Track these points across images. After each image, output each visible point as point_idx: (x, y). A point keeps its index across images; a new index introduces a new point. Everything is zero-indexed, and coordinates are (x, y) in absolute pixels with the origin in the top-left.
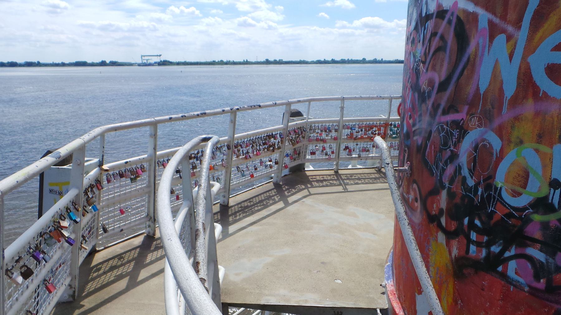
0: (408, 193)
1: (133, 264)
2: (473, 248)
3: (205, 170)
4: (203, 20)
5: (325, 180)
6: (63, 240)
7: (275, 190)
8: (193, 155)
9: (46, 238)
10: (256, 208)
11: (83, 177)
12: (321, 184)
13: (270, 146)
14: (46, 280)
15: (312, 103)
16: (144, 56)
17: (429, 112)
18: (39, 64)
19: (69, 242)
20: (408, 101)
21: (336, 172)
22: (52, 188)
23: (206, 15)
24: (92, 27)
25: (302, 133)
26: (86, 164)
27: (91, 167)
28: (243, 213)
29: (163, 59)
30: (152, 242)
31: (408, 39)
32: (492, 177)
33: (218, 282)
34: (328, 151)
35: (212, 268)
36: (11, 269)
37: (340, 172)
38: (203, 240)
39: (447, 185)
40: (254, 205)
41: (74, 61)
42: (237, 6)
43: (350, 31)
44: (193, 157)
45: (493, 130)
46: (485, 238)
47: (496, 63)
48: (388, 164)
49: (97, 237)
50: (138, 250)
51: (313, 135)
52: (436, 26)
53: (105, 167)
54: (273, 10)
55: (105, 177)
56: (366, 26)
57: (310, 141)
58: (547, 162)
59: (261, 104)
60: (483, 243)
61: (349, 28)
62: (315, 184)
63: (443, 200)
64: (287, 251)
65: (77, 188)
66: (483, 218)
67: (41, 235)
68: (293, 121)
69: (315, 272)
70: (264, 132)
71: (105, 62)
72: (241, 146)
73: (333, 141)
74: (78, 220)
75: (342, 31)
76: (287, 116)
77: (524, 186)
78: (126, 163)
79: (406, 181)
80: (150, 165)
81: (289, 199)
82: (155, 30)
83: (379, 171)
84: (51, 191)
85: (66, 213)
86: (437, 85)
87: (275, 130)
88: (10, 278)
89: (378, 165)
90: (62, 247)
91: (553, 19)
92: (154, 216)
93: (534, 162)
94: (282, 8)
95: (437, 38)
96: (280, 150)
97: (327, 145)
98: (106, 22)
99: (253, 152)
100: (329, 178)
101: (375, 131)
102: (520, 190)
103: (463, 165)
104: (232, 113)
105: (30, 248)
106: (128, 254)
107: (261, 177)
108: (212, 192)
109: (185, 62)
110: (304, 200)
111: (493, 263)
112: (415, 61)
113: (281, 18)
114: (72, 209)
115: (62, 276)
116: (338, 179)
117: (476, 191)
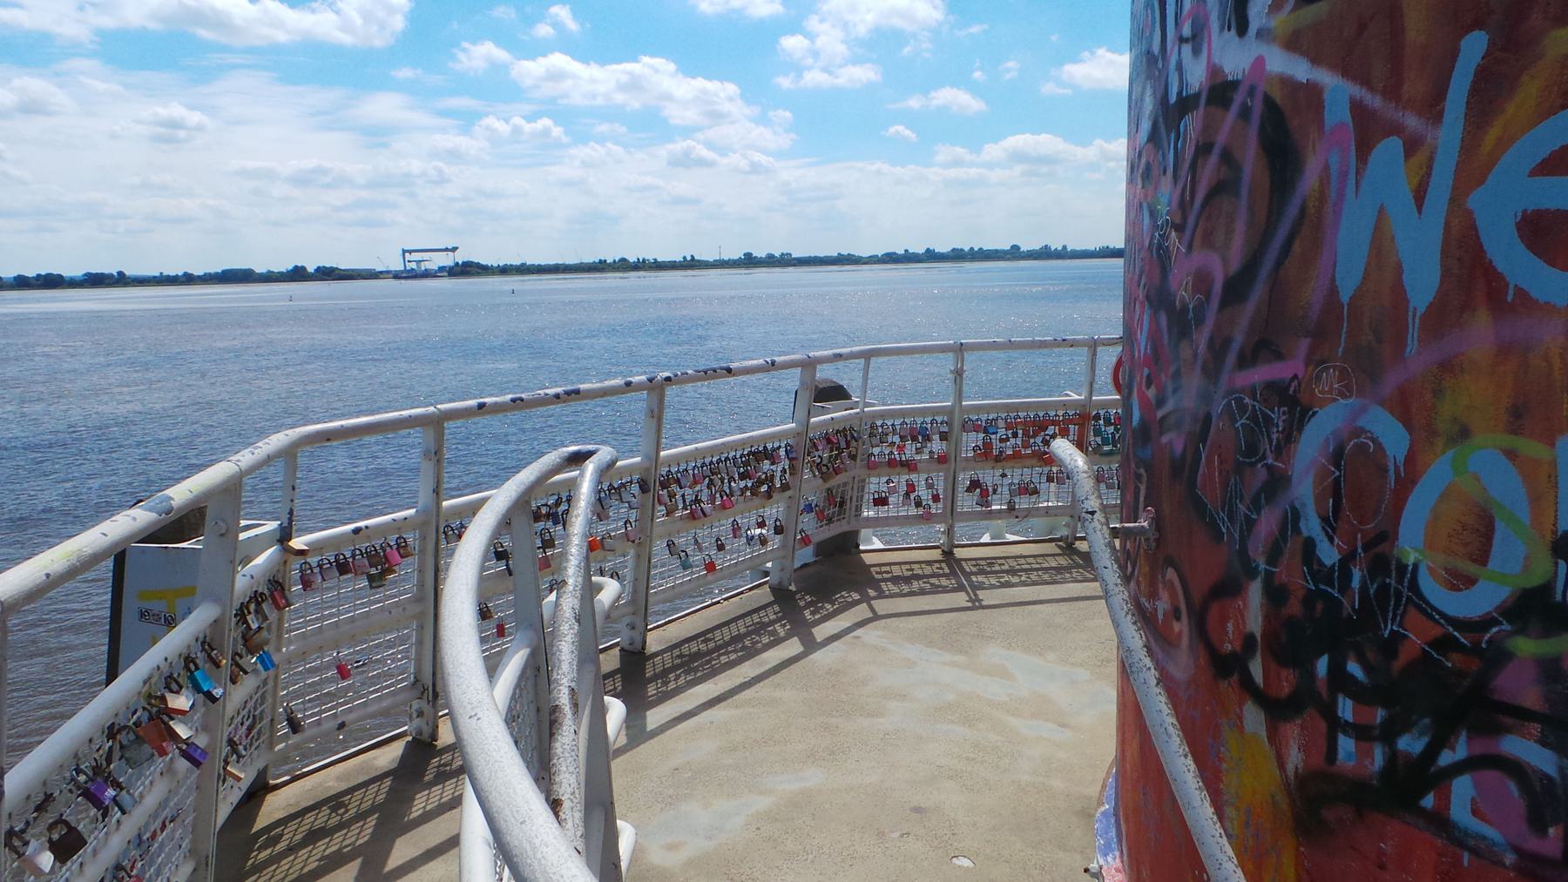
0: (1153, 595)
1: (372, 821)
2: (1346, 744)
3: (576, 540)
4: (573, 151)
5: (918, 577)
6: (173, 750)
7: (777, 608)
8: (544, 511)
9: (125, 742)
10: (724, 659)
11: (234, 572)
12: (906, 589)
13: (761, 482)
14: (123, 868)
15: (873, 360)
16: (410, 252)
17: (1199, 363)
18: (121, 280)
19: (192, 755)
20: (1142, 337)
21: (948, 554)
22: (146, 605)
23: (581, 138)
25: (848, 446)
26: (243, 536)
27: (258, 544)
28: (687, 673)
29: (460, 257)
30: (430, 762)
31: (1132, 168)
32: (1386, 536)
33: (617, 866)
34: (924, 493)
35: (599, 816)
36: (23, 831)
37: (959, 553)
38: (572, 736)
39: (1262, 566)
40: (717, 648)
41: (1091, 246)
43: (973, 172)
44: (542, 512)
45: (1382, 403)
46: (1380, 714)
47: (1384, 218)
48: (1093, 513)
49: (271, 746)
50: (388, 782)
52: (1208, 128)
53: (297, 543)
54: (762, 120)
55: (296, 574)
56: (1018, 157)
57: (871, 466)
58: (1542, 484)
59: (733, 366)
60: (1373, 727)
61: (971, 165)
62: (888, 587)
63: (1253, 610)
64: (813, 777)
65: (217, 600)
66: (1370, 655)
67: (112, 732)
68: (824, 411)
69: (896, 835)
70: (743, 442)
71: (303, 268)
72: (678, 481)
73: (935, 466)
74: (217, 692)
75: (953, 173)
76: (805, 397)
77: (1482, 558)
78: (357, 531)
79: (1145, 561)
80: (423, 538)
81: (815, 630)
83: (1068, 547)
84: (143, 615)
85: (184, 672)
86: (1218, 287)
87: (773, 436)
88: (20, 855)
89: (1065, 532)
90: (169, 770)
91: (1530, 90)
92: (434, 685)
93: (1504, 486)
94: (788, 114)
95: (1213, 159)
96: (788, 493)
97: (919, 479)
98: (311, 163)
100: (928, 570)
102: (1472, 569)
103: (1304, 505)
104: (650, 390)
105: (79, 771)
106: (358, 794)
107: (735, 571)
108: (597, 610)
110: (859, 632)
111: (1408, 786)
112: (1155, 227)
113: (785, 141)
114: (200, 662)
115: (169, 856)
116: (953, 574)
117: (1346, 576)
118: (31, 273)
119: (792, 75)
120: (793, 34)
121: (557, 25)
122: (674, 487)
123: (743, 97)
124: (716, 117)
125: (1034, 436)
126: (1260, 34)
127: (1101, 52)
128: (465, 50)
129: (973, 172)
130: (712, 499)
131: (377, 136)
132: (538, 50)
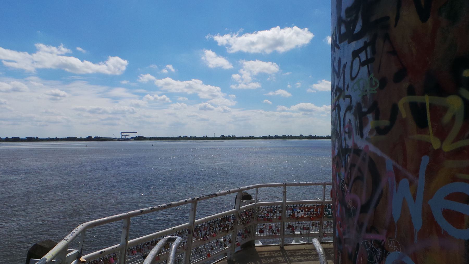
4: (172, 105)
5: (273, 257)
13: (225, 228)
16: (123, 133)
18: (37, 139)
21: (282, 248)
23: (175, 101)
24: (83, 110)
25: (251, 214)
26: (68, 255)
29: (138, 135)
42: (199, 95)
43: (288, 113)
47: (405, 200)
51: (261, 216)
54: (227, 97)
56: (301, 110)
57: (259, 221)
59: (218, 193)
61: (287, 111)
70: (220, 216)
71: (91, 137)
78: (101, 253)
80: (121, 253)
82: (134, 112)
86: (359, 207)
94: (234, 96)
96: (233, 230)
97: (273, 224)
99: (210, 234)
100: (276, 254)
101: (313, 211)
107: (218, 256)
109: (156, 137)
113: (234, 103)
116: (283, 256)
118: (10, 137)
119: (236, 85)
120: (235, 74)
121: (168, 70)
122: (199, 231)
123: (221, 91)
124: (214, 96)
125: (308, 211)
126: (367, 139)
127: (323, 81)
128: (142, 76)
129: (288, 113)
130: (210, 234)
131: (116, 99)
132: (164, 76)
